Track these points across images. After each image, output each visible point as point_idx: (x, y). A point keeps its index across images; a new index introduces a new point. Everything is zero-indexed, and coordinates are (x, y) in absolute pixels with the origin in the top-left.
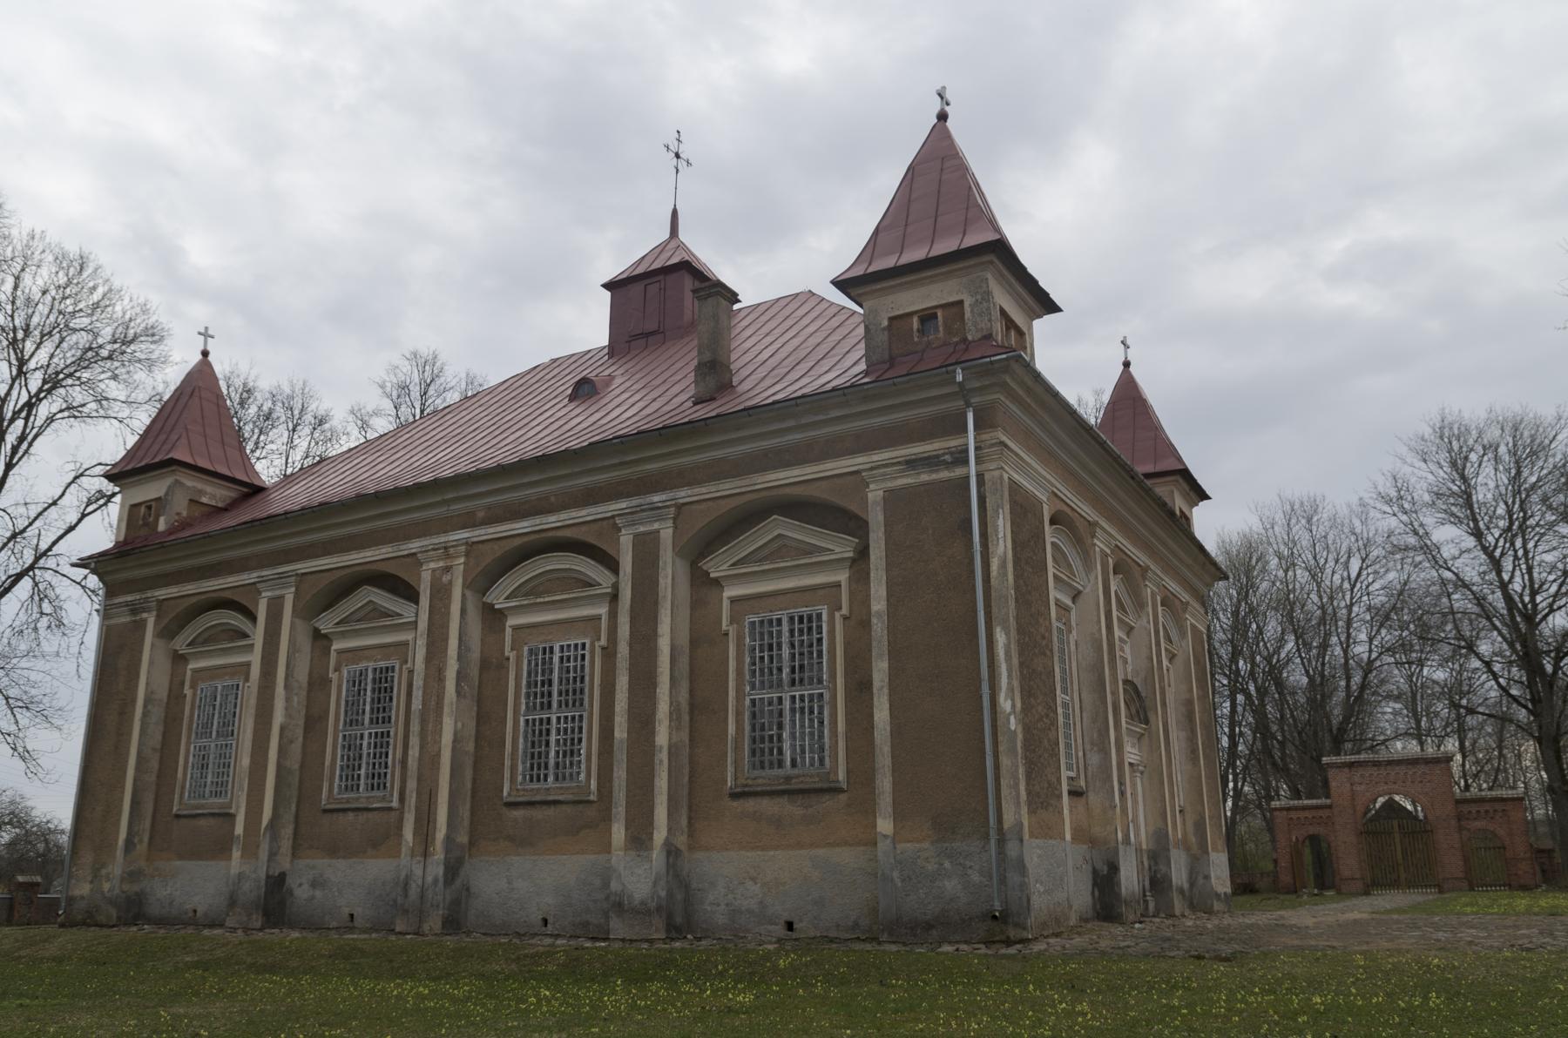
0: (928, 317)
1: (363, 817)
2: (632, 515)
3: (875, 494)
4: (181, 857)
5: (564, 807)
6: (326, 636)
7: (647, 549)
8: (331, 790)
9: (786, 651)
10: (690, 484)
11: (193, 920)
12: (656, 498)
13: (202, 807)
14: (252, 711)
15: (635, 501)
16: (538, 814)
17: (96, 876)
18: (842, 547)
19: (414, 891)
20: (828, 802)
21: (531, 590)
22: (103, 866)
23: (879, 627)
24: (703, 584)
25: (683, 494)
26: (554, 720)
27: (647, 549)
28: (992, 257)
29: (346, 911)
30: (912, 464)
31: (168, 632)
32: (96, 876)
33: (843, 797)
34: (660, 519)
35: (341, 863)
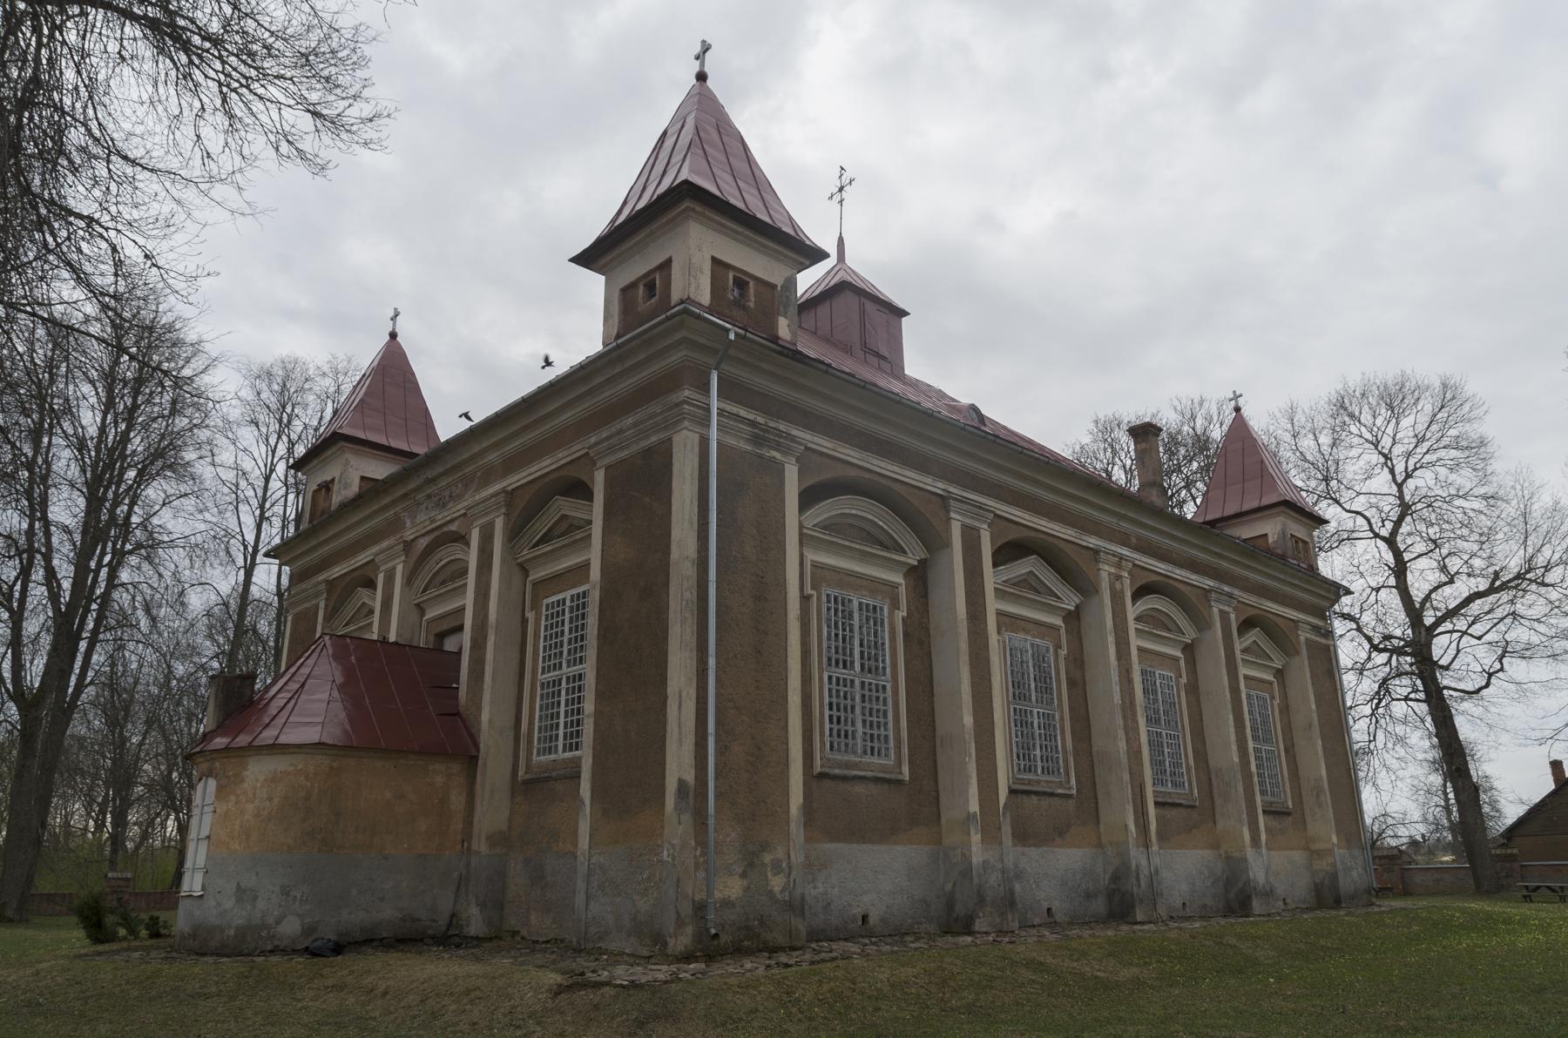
1: (1046, 801)
4: (834, 837)
5: (1182, 810)
11: (862, 929)
13: (856, 766)
14: (966, 658)
17: (751, 863)
18: (1070, 601)
22: (765, 847)
26: (857, 682)
28: (687, 204)
29: (1045, 905)
32: (751, 863)
33: (1071, 802)
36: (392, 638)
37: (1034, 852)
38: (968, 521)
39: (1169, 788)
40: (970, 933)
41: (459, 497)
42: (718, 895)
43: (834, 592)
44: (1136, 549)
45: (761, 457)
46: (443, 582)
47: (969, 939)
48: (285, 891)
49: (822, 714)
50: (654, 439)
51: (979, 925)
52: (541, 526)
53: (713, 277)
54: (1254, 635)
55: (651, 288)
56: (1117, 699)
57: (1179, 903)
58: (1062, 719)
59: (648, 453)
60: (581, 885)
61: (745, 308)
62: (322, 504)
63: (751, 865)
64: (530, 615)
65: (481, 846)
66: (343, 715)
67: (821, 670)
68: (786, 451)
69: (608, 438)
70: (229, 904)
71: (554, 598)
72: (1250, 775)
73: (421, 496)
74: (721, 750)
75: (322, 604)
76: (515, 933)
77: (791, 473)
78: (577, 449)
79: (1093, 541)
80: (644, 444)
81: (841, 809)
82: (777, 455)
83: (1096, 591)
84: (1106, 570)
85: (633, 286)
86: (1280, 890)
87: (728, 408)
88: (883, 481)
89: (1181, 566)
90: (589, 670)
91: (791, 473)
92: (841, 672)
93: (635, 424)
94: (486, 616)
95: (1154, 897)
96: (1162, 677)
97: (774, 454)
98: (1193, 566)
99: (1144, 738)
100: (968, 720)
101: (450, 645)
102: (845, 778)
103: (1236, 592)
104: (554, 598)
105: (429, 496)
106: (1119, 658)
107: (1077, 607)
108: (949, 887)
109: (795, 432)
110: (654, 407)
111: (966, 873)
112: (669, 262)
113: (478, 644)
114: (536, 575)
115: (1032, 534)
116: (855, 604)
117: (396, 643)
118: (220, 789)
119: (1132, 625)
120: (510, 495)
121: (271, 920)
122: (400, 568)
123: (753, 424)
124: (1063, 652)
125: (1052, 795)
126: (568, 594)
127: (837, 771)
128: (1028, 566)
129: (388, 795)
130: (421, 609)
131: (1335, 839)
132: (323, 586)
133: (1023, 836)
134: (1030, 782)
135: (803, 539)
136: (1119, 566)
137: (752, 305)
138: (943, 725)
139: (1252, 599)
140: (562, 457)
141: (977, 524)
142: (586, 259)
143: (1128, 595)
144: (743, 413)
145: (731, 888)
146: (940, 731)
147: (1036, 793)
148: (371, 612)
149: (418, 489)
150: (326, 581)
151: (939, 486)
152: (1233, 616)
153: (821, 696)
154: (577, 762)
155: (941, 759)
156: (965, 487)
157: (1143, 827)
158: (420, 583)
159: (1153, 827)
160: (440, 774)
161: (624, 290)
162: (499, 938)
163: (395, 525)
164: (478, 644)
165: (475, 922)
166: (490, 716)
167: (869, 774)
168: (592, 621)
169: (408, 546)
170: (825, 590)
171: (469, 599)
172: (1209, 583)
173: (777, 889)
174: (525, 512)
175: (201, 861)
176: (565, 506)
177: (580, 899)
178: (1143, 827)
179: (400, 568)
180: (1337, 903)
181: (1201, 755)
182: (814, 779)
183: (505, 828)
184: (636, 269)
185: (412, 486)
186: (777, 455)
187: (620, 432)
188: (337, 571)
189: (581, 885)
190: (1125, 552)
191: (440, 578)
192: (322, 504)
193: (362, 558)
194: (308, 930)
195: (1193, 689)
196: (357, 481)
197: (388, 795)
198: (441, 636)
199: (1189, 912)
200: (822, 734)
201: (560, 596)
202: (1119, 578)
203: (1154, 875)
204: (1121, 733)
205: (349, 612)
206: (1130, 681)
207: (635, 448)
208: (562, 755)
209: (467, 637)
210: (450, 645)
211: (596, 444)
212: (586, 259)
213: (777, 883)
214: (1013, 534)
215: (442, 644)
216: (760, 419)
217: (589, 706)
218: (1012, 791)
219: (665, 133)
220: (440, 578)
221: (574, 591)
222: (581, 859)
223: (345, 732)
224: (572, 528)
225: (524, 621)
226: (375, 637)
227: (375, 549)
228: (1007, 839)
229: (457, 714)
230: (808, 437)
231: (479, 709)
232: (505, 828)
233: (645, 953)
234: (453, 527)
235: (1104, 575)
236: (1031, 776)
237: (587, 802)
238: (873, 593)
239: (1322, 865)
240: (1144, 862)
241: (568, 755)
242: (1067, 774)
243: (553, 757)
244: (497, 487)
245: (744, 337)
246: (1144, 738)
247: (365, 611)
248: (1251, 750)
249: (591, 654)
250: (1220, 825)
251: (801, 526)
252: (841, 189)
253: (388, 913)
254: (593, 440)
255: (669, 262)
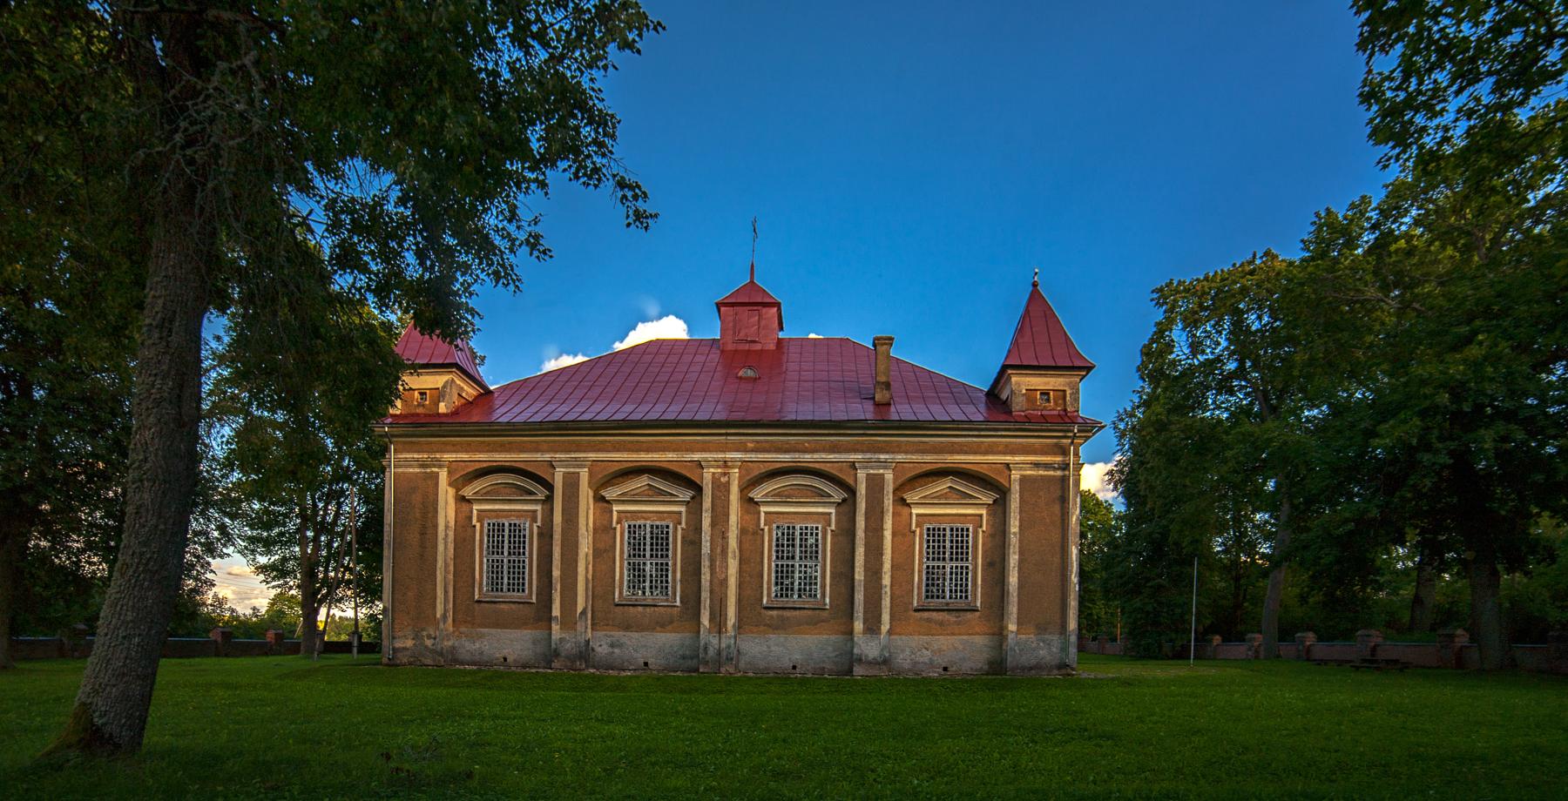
0: (1045, 393)
2: (867, 464)
3: (1015, 475)
6: (469, 501)
7: (572, 483)
8: (622, 591)
9: (948, 544)
10: (906, 452)
12: (882, 456)
15: (868, 456)
16: (787, 613)
18: (686, 495)
19: (711, 652)
20: (969, 615)
21: (781, 497)
23: (1014, 540)
24: (749, 503)
25: (900, 457)
27: (875, 484)
30: (1037, 465)
31: (458, 483)
34: (440, 467)
35: (635, 635)
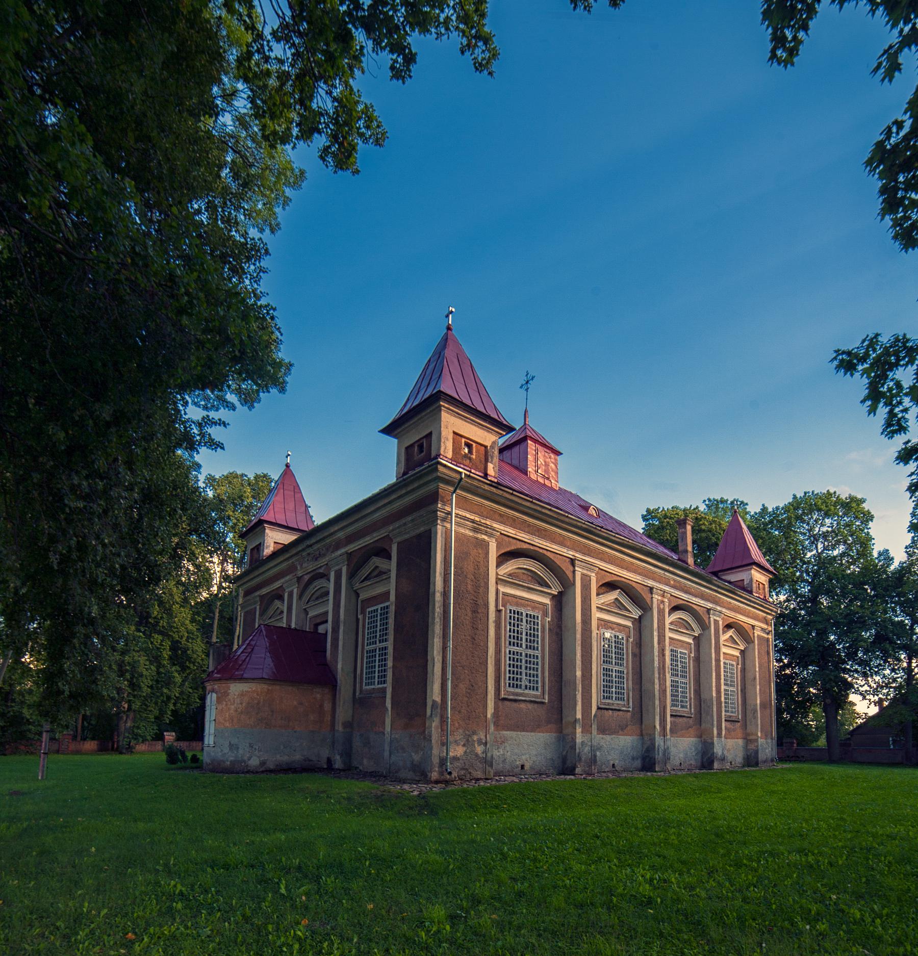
13: (521, 695)
18: (636, 613)
29: (612, 763)
36: (293, 626)
37: (608, 738)
38: (585, 572)
39: (679, 708)
40: (574, 775)
41: (324, 555)
42: (451, 754)
43: (513, 608)
44: (674, 587)
45: (477, 539)
46: (317, 599)
47: (572, 777)
48: (251, 746)
49: (505, 627)
50: (422, 529)
51: (578, 770)
52: (365, 572)
53: (454, 442)
54: (731, 633)
55: (421, 447)
56: (656, 664)
57: (678, 763)
58: (628, 673)
59: (419, 536)
60: (387, 748)
61: (470, 459)
62: (256, 556)
63: (468, 740)
64: (360, 617)
65: (339, 728)
66: (272, 665)
67: (505, 647)
68: (491, 535)
69: (398, 527)
70: (226, 750)
71: (373, 609)
72: (721, 703)
73: (304, 554)
74: (454, 687)
75: (258, 607)
76: (356, 768)
77: (493, 546)
78: (382, 533)
79: (650, 583)
80: (418, 532)
81: (511, 718)
82: (486, 538)
83: (651, 609)
84: (656, 597)
85: (412, 446)
86: (730, 757)
87: (460, 513)
88: (541, 551)
89: (696, 596)
90: (390, 644)
91: (493, 546)
92: (515, 649)
93: (413, 520)
94: (339, 616)
95: (667, 758)
96: (681, 653)
97: (484, 537)
98: (702, 597)
99: (668, 683)
100: (579, 673)
101: (321, 629)
102: (515, 701)
103: (724, 610)
104: (373, 609)
105: (309, 554)
106: (659, 643)
107: (640, 617)
108: (564, 753)
109: (495, 525)
110: (422, 512)
111: (573, 747)
112: (431, 433)
113: (335, 630)
114: (363, 596)
115: (619, 579)
116: (524, 614)
117: (295, 629)
118: (218, 698)
119: (667, 626)
120: (350, 555)
121: (245, 758)
122: (295, 591)
123: (473, 521)
124: (631, 640)
125: (619, 710)
126: (379, 607)
127: (511, 697)
128: (614, 595)
129: (295, 703)
130: (306, 612)
131: (759, 734)
132: (258, 599)
133: (602, 730)
134: (609, 704)
135: (498, 581)
136: (663, 596)
137: (474, 457)
138: (566, 676)
139: (732, 614)
140: (376, 536)
141: (589, 573)
142: (388, 430)
143: (667, 610)
144: (468, 516)
145: (457, 751)
146: (564, 679)
147: (612, 709)
148: (282, 612)
149: (303, 550)
150: (260, 596)
151: (570, 553)
152: (721, 623)
153: (505, 662)
154: (384, 690)
155: (564, 692)
156: (584, 554)
157: (663, 727)
158: (306, 598)
159: (668, 727)
160: (319, 694)
161: (407, 448)
162: (349, 770)
163: (292, 569)
164: (335, 630)
165: (338, 763)
166: (341, 667)
167: (527, 699)
168: (391, 621)
169: (299, 579)
170: (509, 607)
171: (330, 607)
172: (710, 605)
173: (479, 752)
174: (357, 562)
175: (212, 731)
176: (376, 561)
177: (386, 754)
178: (663, 727)
179: (295, 591)
180: (757, 764)
181: (698, 692)
182: (498, 699)
183: (350, 720)
184: (413, 437)
185: (300, 548)
186: (486, 538)
187: (405, 524)
188: (264, 591)
189: (387, 748)
190: (667, 588)
191: (315, 596)
192: (256, 556)
193: (277, 585)
194: (263, 763)
195: (697, 659)
196: (272, 544)
197: (295, 703)
198: (317, 625)
199: (682, 767)
200: (505, 679)
201: (375, 608)
202: (663, 602)
203: (666, 751)
204: (657, 681)
205: (271, 612)
206: (664, 655)
207: (413, 534)
208: (377, 686)
209: (329, 625)
210: (321, 629)
211: (393, 530)
212: (388, 430)
213: (479, 749)
214: (608, 579)
215: (317, 629)
216: (477, 519)
217: (390, 663)
218: (599, 708)
219: (430, 360)
220: (315, 596)
221: (382, 605)
222: (387, 735)
223: (273, 673)
224: (381, 573)
225: (358, 620)
226: (284, 626)
227: (282, 580)
228: (594, 732)
229: (327, 665)
230: (502, 528)
231: (337, 662)
232: (350, 720)
233: (417, 778)
234: (321, 571)
235: (655, 601)
236: (610, 701)
237: (390, 709)
238: (534, 608)
239: (752, 747)
240: (662, 744)
241: (380, 686)
242: (628, 700)
243: (373, 687)
244: (343, 550)
245: (469, 476)
246: (668, 683)
247: (279, 611)
248: (722, 690)
249: (391, 637)
250: (703, 725)
251: (497, 574)
252: (527, 382)
253: (298, 757)
254: (391, 528)
255: (431, 433)
